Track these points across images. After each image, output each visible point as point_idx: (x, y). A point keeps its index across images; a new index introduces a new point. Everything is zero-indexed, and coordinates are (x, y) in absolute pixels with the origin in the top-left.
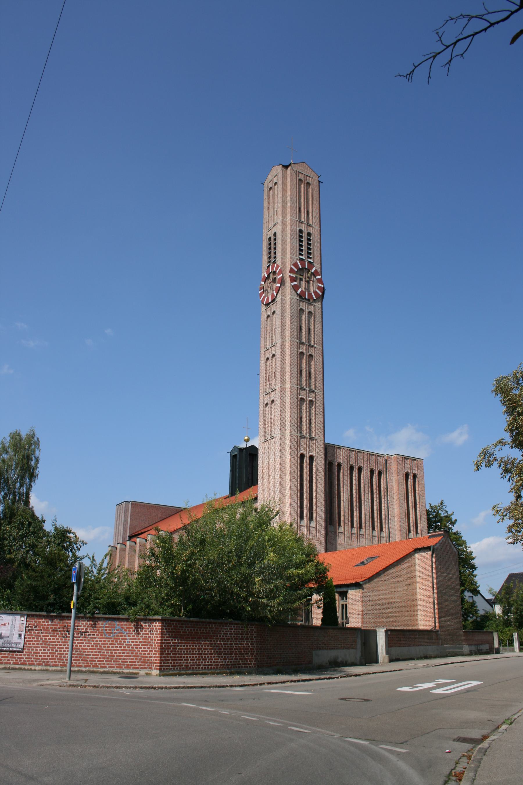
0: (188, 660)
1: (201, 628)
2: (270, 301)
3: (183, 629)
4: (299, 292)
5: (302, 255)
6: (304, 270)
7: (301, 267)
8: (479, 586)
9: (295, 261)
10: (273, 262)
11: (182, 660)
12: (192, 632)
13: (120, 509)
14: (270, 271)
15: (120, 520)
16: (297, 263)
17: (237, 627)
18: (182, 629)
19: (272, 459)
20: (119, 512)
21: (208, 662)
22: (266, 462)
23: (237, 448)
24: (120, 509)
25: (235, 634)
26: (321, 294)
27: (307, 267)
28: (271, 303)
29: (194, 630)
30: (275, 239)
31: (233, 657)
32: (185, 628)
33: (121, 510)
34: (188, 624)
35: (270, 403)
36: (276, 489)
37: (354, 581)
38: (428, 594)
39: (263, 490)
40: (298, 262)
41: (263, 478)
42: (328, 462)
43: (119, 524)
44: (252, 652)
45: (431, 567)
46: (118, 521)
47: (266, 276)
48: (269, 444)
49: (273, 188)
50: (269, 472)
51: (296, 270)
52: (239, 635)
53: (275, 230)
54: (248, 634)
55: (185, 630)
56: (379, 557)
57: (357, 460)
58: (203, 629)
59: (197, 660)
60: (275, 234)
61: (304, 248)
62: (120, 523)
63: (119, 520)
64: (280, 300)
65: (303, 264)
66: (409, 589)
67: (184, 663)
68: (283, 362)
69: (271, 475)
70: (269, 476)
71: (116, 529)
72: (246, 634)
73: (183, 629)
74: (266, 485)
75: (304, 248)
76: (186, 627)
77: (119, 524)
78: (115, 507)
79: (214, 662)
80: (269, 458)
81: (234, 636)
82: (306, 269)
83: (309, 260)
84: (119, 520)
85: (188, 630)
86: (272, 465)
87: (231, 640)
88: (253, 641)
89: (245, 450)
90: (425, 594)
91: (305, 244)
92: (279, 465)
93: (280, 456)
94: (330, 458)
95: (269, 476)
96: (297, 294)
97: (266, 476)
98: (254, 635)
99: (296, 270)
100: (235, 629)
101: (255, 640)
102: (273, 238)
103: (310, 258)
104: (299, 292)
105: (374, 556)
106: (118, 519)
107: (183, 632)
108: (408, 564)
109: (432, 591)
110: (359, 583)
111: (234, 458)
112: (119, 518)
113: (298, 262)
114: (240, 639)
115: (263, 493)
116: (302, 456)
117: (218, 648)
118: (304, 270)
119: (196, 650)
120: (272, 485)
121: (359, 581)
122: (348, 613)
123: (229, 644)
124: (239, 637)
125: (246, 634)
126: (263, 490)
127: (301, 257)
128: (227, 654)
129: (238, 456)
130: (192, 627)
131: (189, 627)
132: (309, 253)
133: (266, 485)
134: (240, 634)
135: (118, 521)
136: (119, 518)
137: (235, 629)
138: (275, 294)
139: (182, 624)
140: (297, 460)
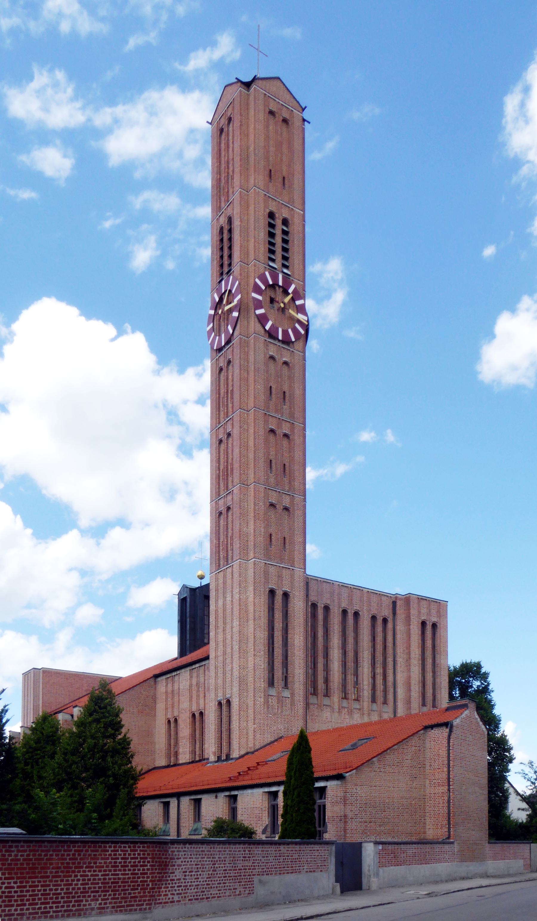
0: (25, 905)
1: (49, 851)
2: (223, 344)
3: (13, 854)
4: (267, 327)
5: (273, 260)
6: (277, 288)
7: (271, 283)
8: (515, 758)
9: (262, 271)
10: (228, 273)
11: (13, 906)
12: (31, 860)
13: (28, 680)
14: (223, 291)
15: (29, 696)
16: (264, 274)
17: (115, 847)
18: (10, 855)
19: (229, 598)
20: (26, 684)
21: (62, 907)
22: (220, 603)
23: (187, 587)
24: (28, 680)
25: (112, 859)
26: (303, 332)
27: (280, 283)
28: (224, 346)
29: (34, 855)
30: (230, 231)
31: (110, 895)
32: (15, 853)
33: (29, 681)
34: (22, 846)
35: (224, 512)
36: (234, 643)
37: (335, 773)
38: (441, 791)
39: (217, 644)
40: (267, 274)
41: (217, 627)
42: (310, 604)
43: (28, 700)
44: (143, 885)
45: (446, 752)
46: (26, 697)
47: (217, 299)
48: (225, 577)
49: (225, 130)
50: (225, 618)
51: (263, 287)
52: (120, 860)
53: (229, 212)
54: (137, 858)
55: (16, 855)
56: (374, 738)
57: (351, 601)
58: (51, 853)
59: (42, 904)
60: (230, 220)
61: (278, 249)
62: (29, 699)
63: (28, 695)
64: (238, 341)
65: (275, 277)
66: (414, 784)
67: (16, 910)
68: (244, 446)
69: (227, 622)
70: (225, 623)
71: (24, 707)
72: (132, 858)
73: (13, 854)
74: (220, 637)
75: (278, 249)
76: (19, 851)
77: (28, 700)
78: (22, 676)
79: (74, 906)
80: (225, 597)
81: (111, 863)
82: (279, 286)
83: (285, 271)
84: (28, 695)
85: (21, 856)
86: (229, 607)
87: (105, 868)
88: (146, 868)
89: (197, 590)
90: (437, 791)
91: (278, 240)
92: (238, 607)
93: (240, 593)
94: (313, 598)
95: (225, 623)
96: (265, 330)
97: (221, 624)
98: (146, 858)
99: (263, 287)
100: (112, 851)
101: (149, 867)
102: (226, 228)
103: (287, 267)
104: (267, 327)
105: (367, 737)
106: (26, 694)
107: (12, 860)
108: (414, 748)
109: (447, 787)
110: (341, 774)
111: (183, 602)
112: (28, 692)
113: (267, 274)
114: (122, 866)
115: (216, 650)
116: (272, 592)
117: (81, 882)
118: (277, 288)
119: (39, 888)
120: (229, 637)
121: (342, 772)
122: (326, 818)
123: (102, 875)
124: (120, 863)
125: (132, 858)
126: (217, 644)
127: (271, 264)
128: (98, 892)
129: (188, 600)
130: (30, 851)
131: (25, 851)
132: (285, 258)
133: (220, 637)
134: (122, 859)
135: (26, 697)
136: (28, 692)
137: (112, 851)
138: (231, 331)
139: (11, 847)
140: (263, 600)
